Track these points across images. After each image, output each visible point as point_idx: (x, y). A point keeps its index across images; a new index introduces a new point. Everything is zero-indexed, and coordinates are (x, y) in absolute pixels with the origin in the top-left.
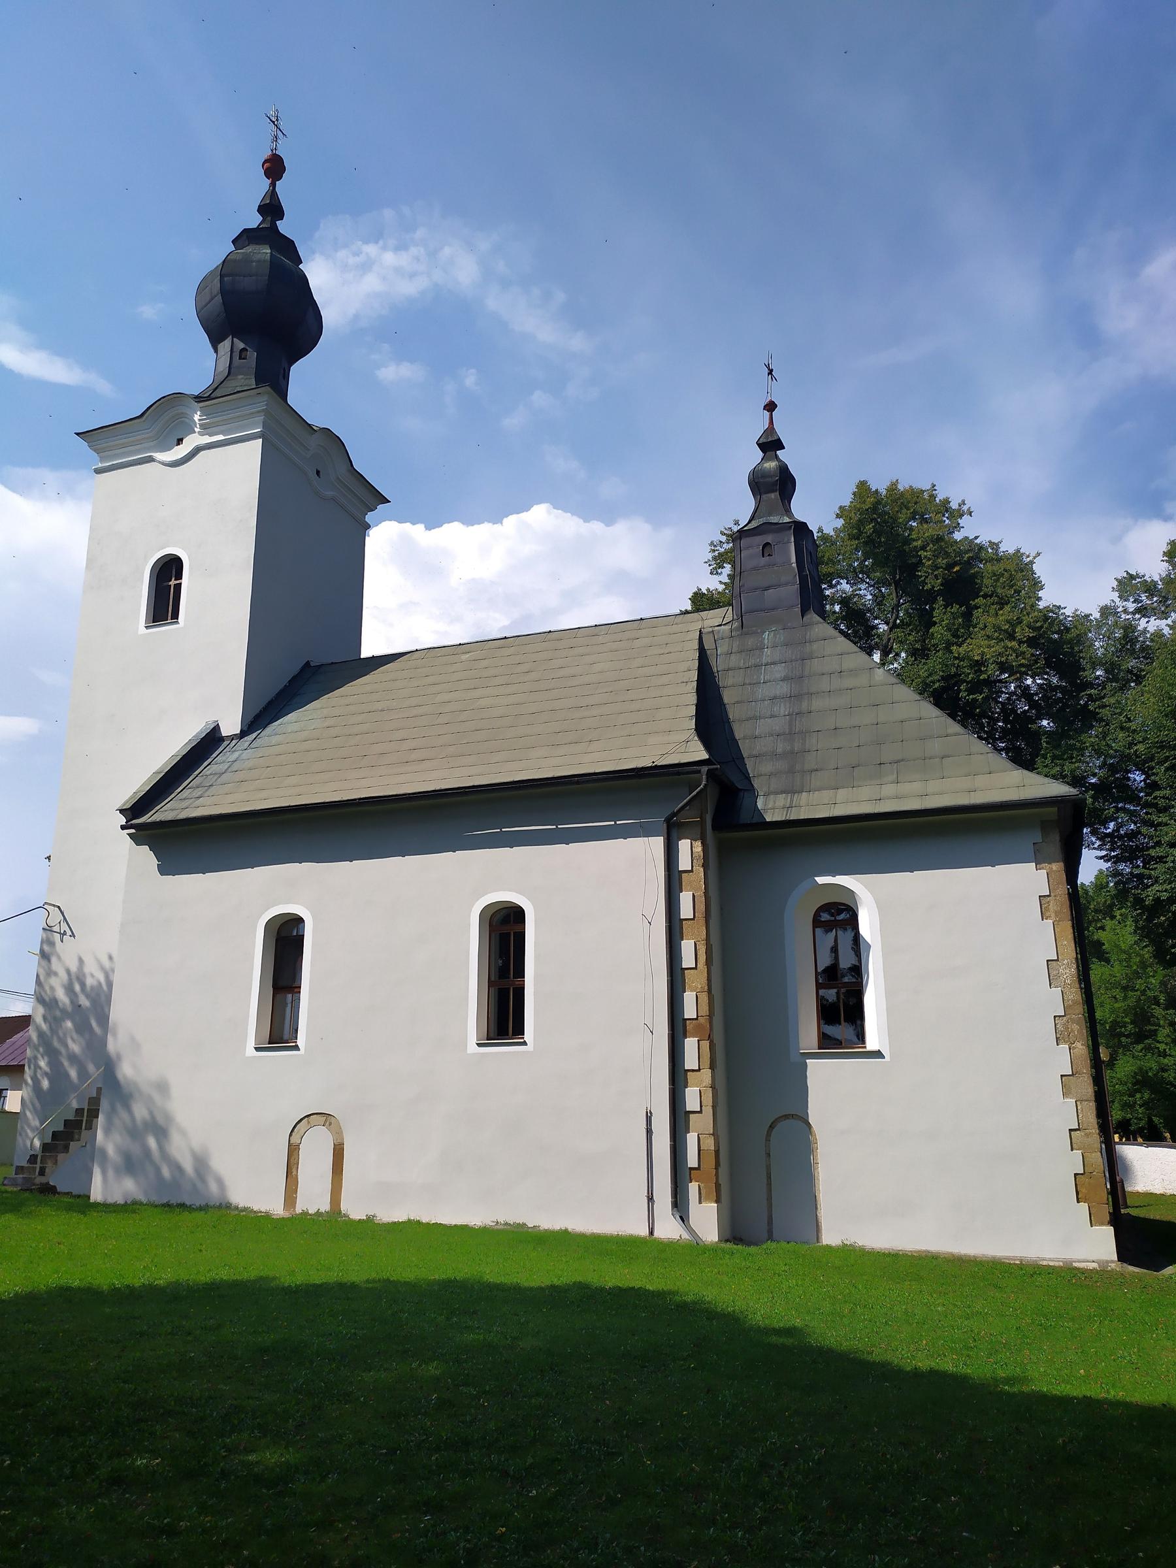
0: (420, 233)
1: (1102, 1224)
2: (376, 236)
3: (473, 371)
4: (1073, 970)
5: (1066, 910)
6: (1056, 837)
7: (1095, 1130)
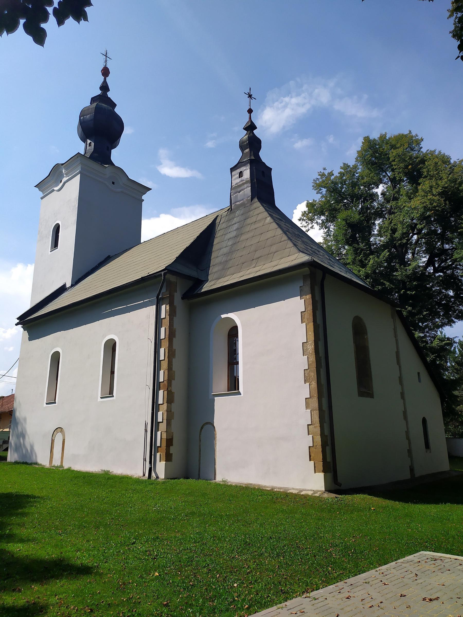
0: (305, 87)
1: (319, 472)
2: (288, 93)
3: (332, 136)
4: (313, 346)
5: (311, 318)
6: (309, 282)
7: (318, 425)
